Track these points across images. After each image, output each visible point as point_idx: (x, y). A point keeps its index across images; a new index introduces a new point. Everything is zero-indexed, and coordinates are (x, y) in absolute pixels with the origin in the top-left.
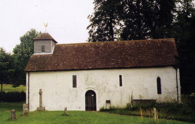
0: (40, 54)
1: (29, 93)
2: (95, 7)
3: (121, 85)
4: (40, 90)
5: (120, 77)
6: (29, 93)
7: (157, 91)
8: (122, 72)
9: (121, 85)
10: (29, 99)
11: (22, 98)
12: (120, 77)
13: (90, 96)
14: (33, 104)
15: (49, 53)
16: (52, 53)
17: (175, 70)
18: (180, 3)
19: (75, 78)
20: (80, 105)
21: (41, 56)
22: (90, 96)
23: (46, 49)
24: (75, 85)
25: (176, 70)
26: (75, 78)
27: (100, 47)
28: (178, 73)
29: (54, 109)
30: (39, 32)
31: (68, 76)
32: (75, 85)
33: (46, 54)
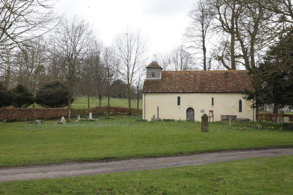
0: (151, 79)
1: (145, 108)
3: (213, 104)
4: (158, 107)
5: (213, 98)
6: (145, 108)
8: (215, 96)
9: (213, 104)
11: (139, 112)
12: (213, 98)
13: (190, 110)
14: (148, 116)
15: (158, 79)
16: (160, 79)
17: (160, 117)
19: (179, 98)
20: (183, 116)
21: (152, 80)
22: (190, 110)
24: (179, 103)
26: (179, 98)
27: (198, 75)
29: (235, 114)
30: (60, 14)
31: (174, 97)
32: (179, 103)
33: (156, 79)
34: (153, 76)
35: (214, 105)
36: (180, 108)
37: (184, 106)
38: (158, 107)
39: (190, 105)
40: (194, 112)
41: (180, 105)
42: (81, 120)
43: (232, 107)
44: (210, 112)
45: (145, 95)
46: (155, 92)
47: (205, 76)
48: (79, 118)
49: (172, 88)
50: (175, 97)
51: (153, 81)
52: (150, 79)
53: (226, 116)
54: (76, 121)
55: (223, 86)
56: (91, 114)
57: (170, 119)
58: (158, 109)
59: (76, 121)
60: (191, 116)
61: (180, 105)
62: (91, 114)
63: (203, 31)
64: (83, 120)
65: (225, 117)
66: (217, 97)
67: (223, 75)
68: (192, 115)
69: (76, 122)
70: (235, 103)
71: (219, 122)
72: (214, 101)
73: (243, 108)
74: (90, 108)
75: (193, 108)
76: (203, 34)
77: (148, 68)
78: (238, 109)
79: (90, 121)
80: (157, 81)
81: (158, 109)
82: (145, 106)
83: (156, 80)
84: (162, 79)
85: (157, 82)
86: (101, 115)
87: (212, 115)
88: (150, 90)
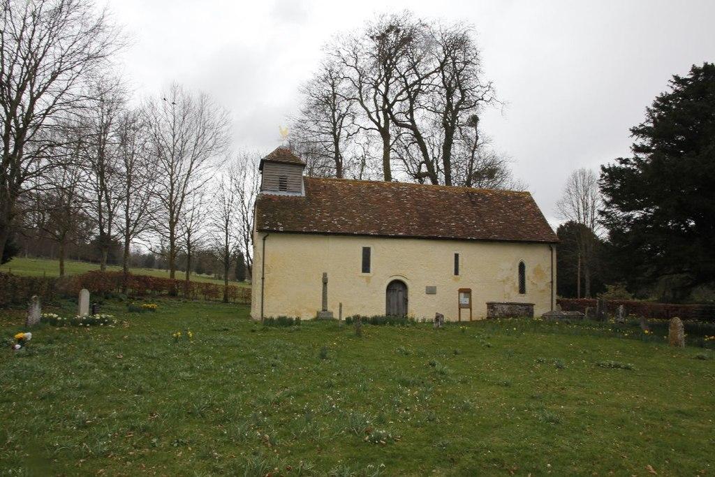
0: (277, 194)
2: (478, 57)
3: (456, 273)
4: (325, 275)
5: (457, 256)
7: (526, 270)
9: (456, 273)
10: (265, 283)
12: (457, 256)
13: (397, 288)
15: (298, 195)
16: (303, 194)
18: (381, 311)
19: (366, 252)
22: (397, 288)
23: (291, 186)
24: (366, 267)
25: (552, 250)
26: (366, 252)
28: (555, 254)
29: (509, 298)
31: (352, 249)
32: (366, 267)
33: (290, 195)
34: (283, 187)
35: (460, 273)
36: (368, 280)
37: (382, 275)
38: (325, 275)
39: (398, 272)
40: (407, 292)
41: (369, 272)
42: (43, 320)
43: (504, 281)
44: (462, 295)
45: (264, 240)
46: (299, 229)
47: (421, 196)
48: (36, 313)
49: (346, 223)
50: (356, 247)
51: (284, 202)
52: (273, 194)
53: (507, 304)
54: (20, 335)
55: (476, 224)
56: (85, 296)
57: (374, 315)
58: (325, 283)
59: (20, 335)
60: (398, 305)
61: (369, 272)
62: (85, 296)
63: (335, 124)
64: (54, 322)
65: (506, 308)
66: (465, 251)
67: (465, 197)
68: (401, 299)
69: (21, 341)
70: (511, 270)
71: (86, 288)
72: (460, 264)
73: (528, 283)
74: (66, 274)
75: (407, 282)
76: (335, 129)
77: (264, 164)
78: (517, 285)
79: (85, 326)
80: (297, 200)
81: (325, 283)
82: (265, 271)
83: (292, 197)
84: (308, 197)
85: (295, 203)
86: (107, 298)
87: (468, 303)
88: (279, 224)
